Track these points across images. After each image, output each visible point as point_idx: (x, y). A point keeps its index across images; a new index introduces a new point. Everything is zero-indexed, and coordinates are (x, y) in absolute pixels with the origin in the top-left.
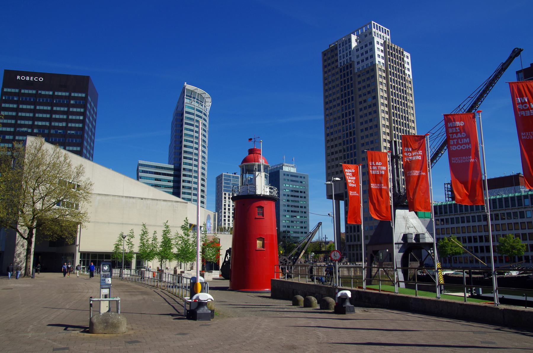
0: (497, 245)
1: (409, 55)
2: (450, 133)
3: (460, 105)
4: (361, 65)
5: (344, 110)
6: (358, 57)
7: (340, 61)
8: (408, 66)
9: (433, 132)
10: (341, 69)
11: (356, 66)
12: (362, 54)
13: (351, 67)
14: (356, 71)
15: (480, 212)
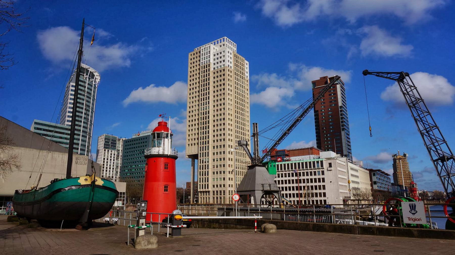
0: (74, 188)
1: (248, 63)
2: (422, 118)
3: (302, 105)
6: (214, 60)
9: (283, 120)
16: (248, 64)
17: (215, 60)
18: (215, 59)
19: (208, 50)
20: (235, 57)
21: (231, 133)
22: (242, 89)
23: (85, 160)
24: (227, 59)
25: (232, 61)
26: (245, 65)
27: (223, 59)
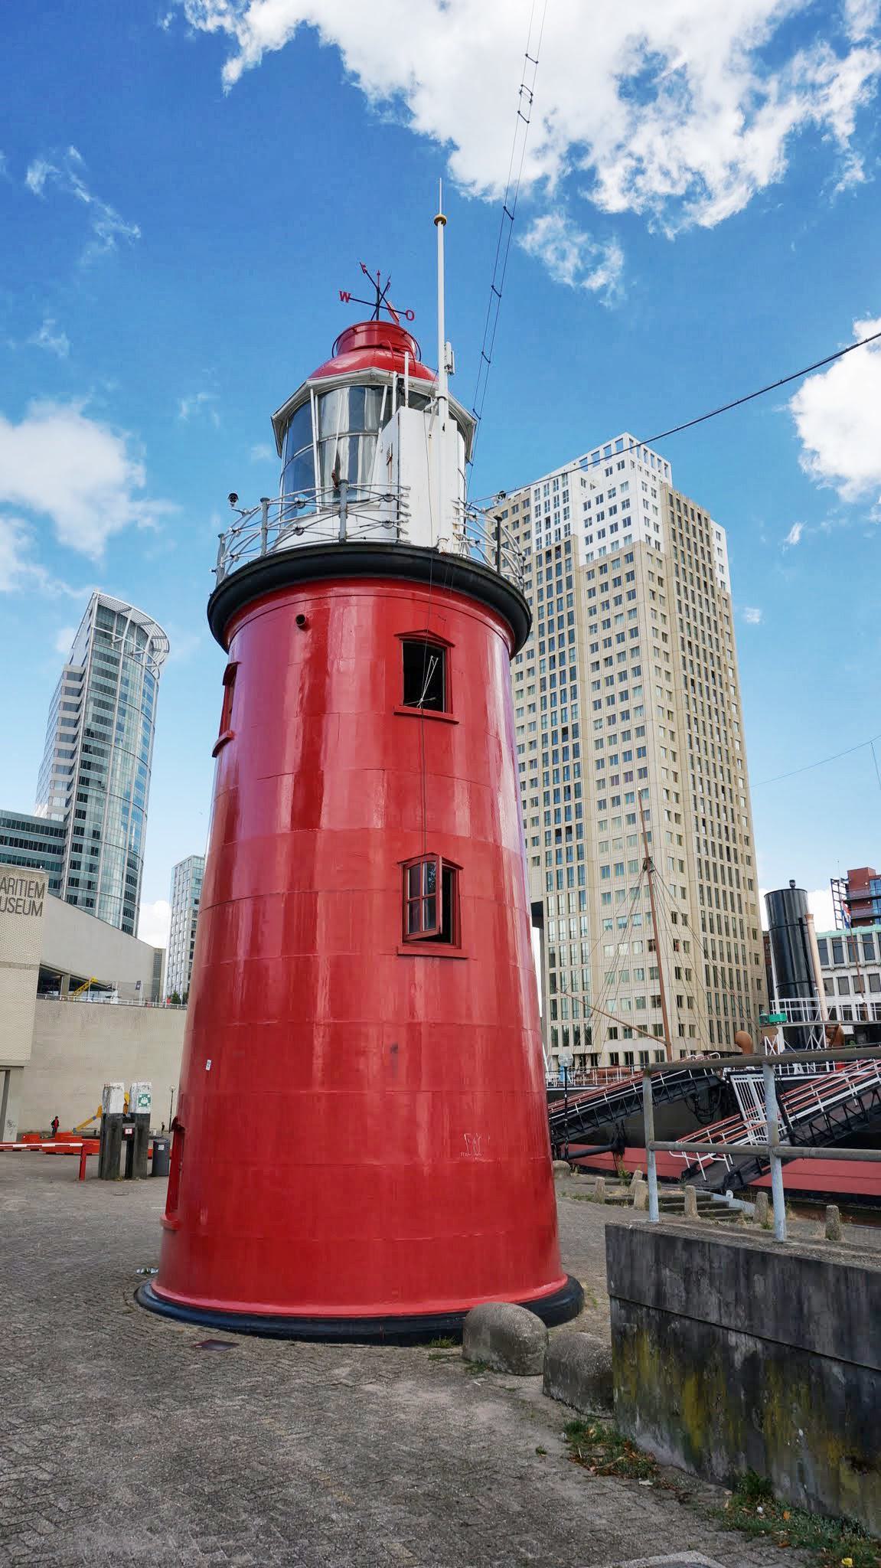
1: (722, 531)
4: (598, 543)
5: (546, 614)
7: (537, 504)
8: (721, 559)
10: (540, 556)
11: (582, 549)
12: (601, 517)
13: (568, 550)
14: (582, 561)
15: (844, 968)
16: (723, 537)
17: (591, 524)
18: (590, 519)
19: (562, 489)
20: (672, 505)
21: (683, 933)
22: (707, 702)
23: (32, 893)
24: (637, 512)
25: (658, 519)
26: (714, 539)
27: (622, 514)
